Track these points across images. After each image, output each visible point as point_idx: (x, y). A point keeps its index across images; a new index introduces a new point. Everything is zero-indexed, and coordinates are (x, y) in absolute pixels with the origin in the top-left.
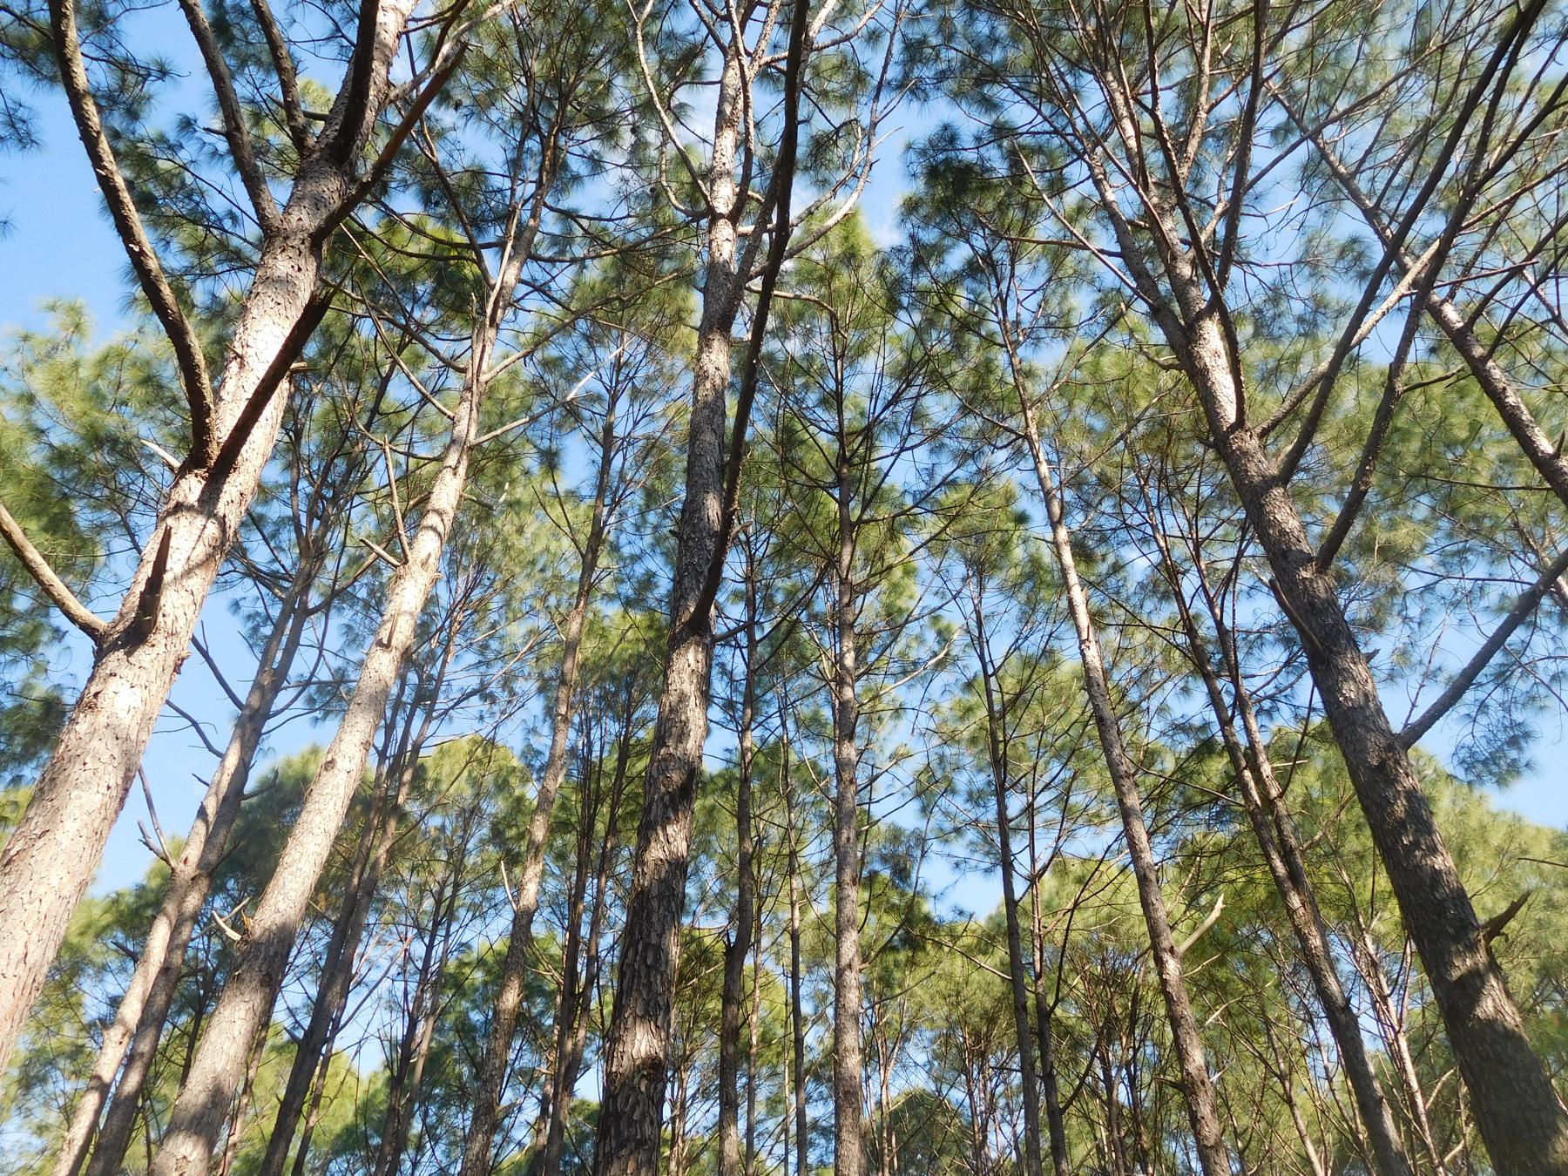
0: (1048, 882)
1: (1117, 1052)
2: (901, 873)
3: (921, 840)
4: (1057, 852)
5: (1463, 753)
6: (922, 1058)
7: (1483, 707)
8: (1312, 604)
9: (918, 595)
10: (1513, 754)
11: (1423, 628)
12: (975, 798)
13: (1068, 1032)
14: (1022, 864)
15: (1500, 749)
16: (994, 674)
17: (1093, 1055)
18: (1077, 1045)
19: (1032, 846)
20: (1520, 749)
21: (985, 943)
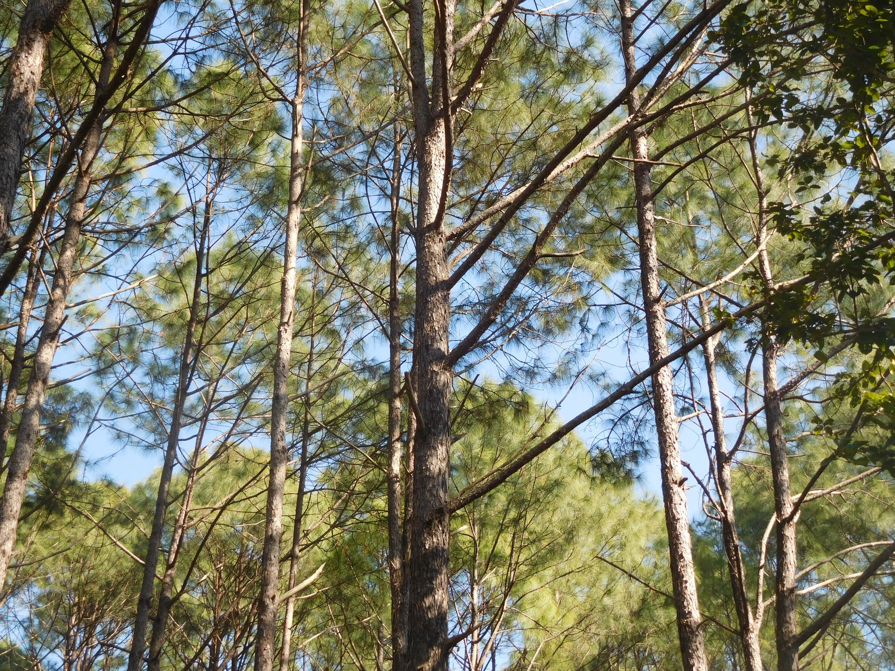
0: (210, 474)
1: (227, 642)
2: (58, 434)
3: (86, 402)
4: (224, 447)
5: (595, 453)
6: (24, 613)
7: (625, 417)
8: (431, 391)
9: (147, 176)
10: (630, 465)
11: (596, 341)
12: (158, 374)
13: (186, 616)
14: (186, 448)
15: (623, 458)
16: (206, 275)
17: (206, 644)
18: (192, 629)
19: (200, 437)
20: (637, 463)
21: (122, 517)
